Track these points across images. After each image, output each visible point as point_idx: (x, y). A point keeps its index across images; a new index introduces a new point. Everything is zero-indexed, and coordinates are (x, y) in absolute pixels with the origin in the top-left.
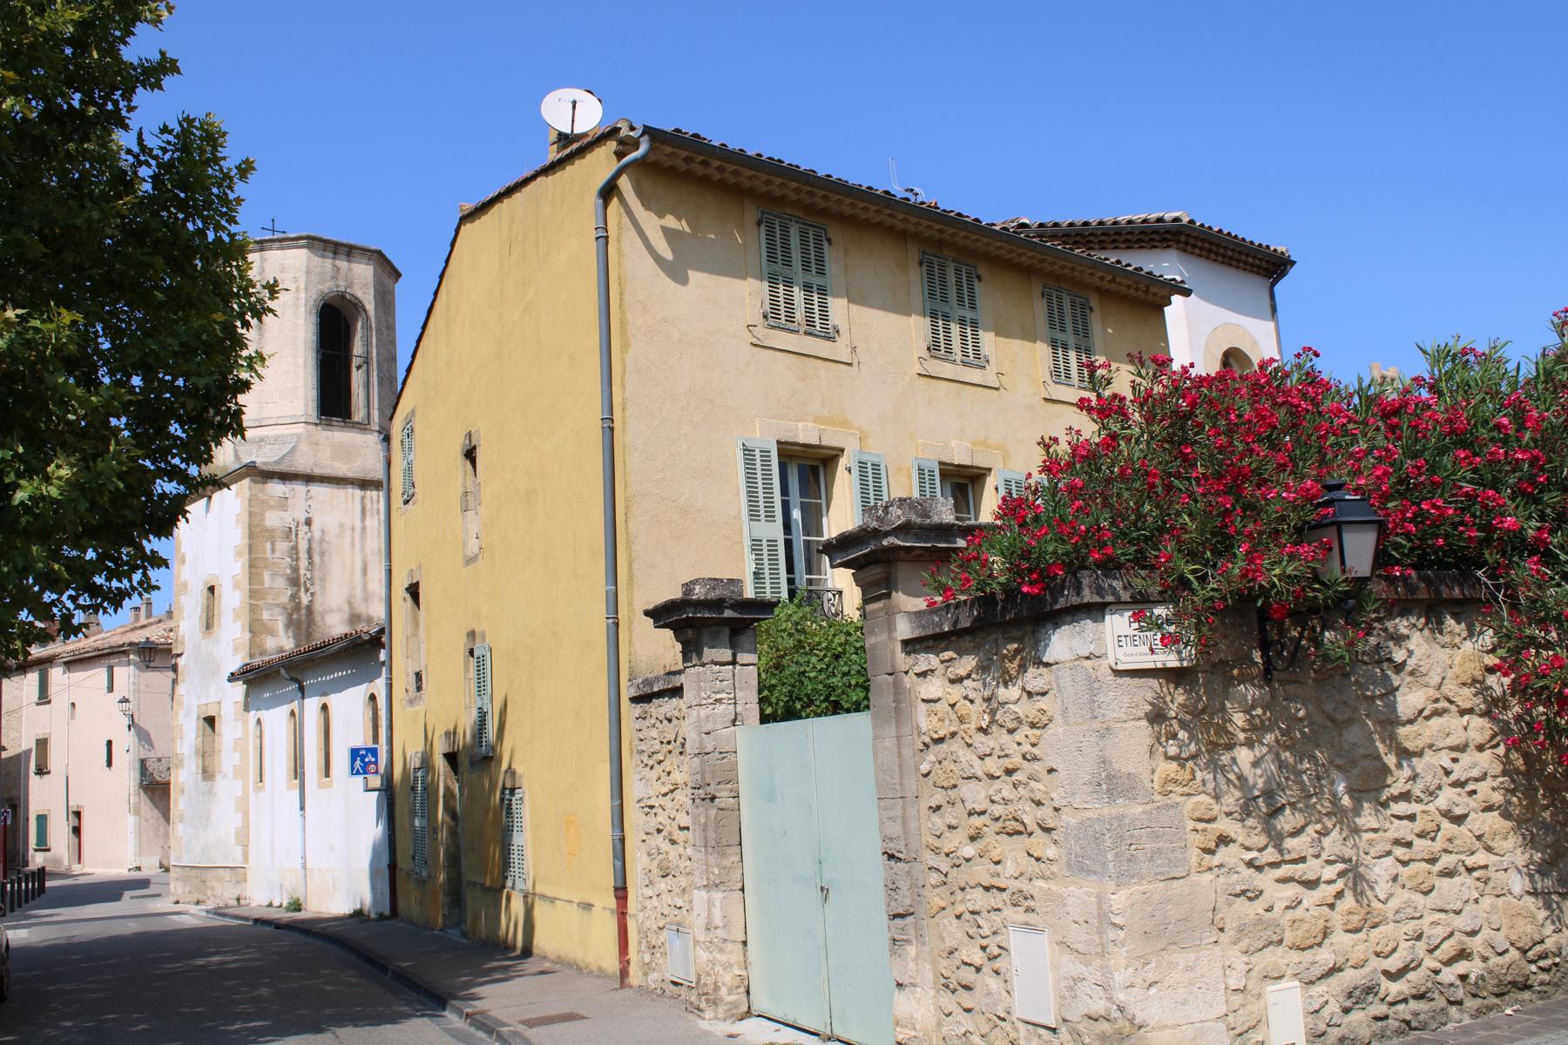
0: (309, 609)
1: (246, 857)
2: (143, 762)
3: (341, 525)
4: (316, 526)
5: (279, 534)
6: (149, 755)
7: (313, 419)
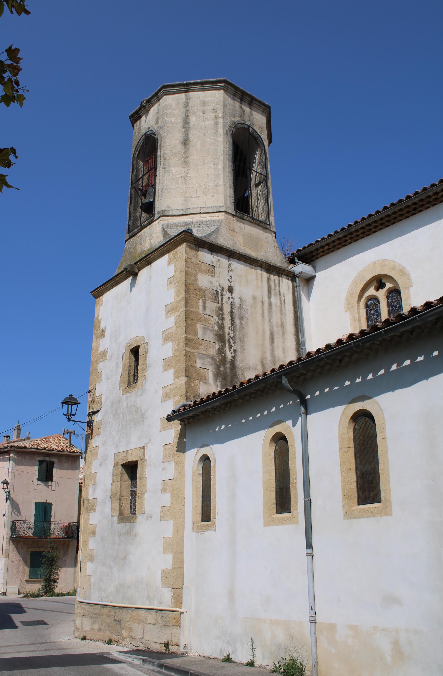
0: (233, 363)
1: (178, 599)
2: (13, 523)
3: (254, 298)
4: (235, 294)
5: (209, 295)
6: (18, 518)
7: (231, 209)
